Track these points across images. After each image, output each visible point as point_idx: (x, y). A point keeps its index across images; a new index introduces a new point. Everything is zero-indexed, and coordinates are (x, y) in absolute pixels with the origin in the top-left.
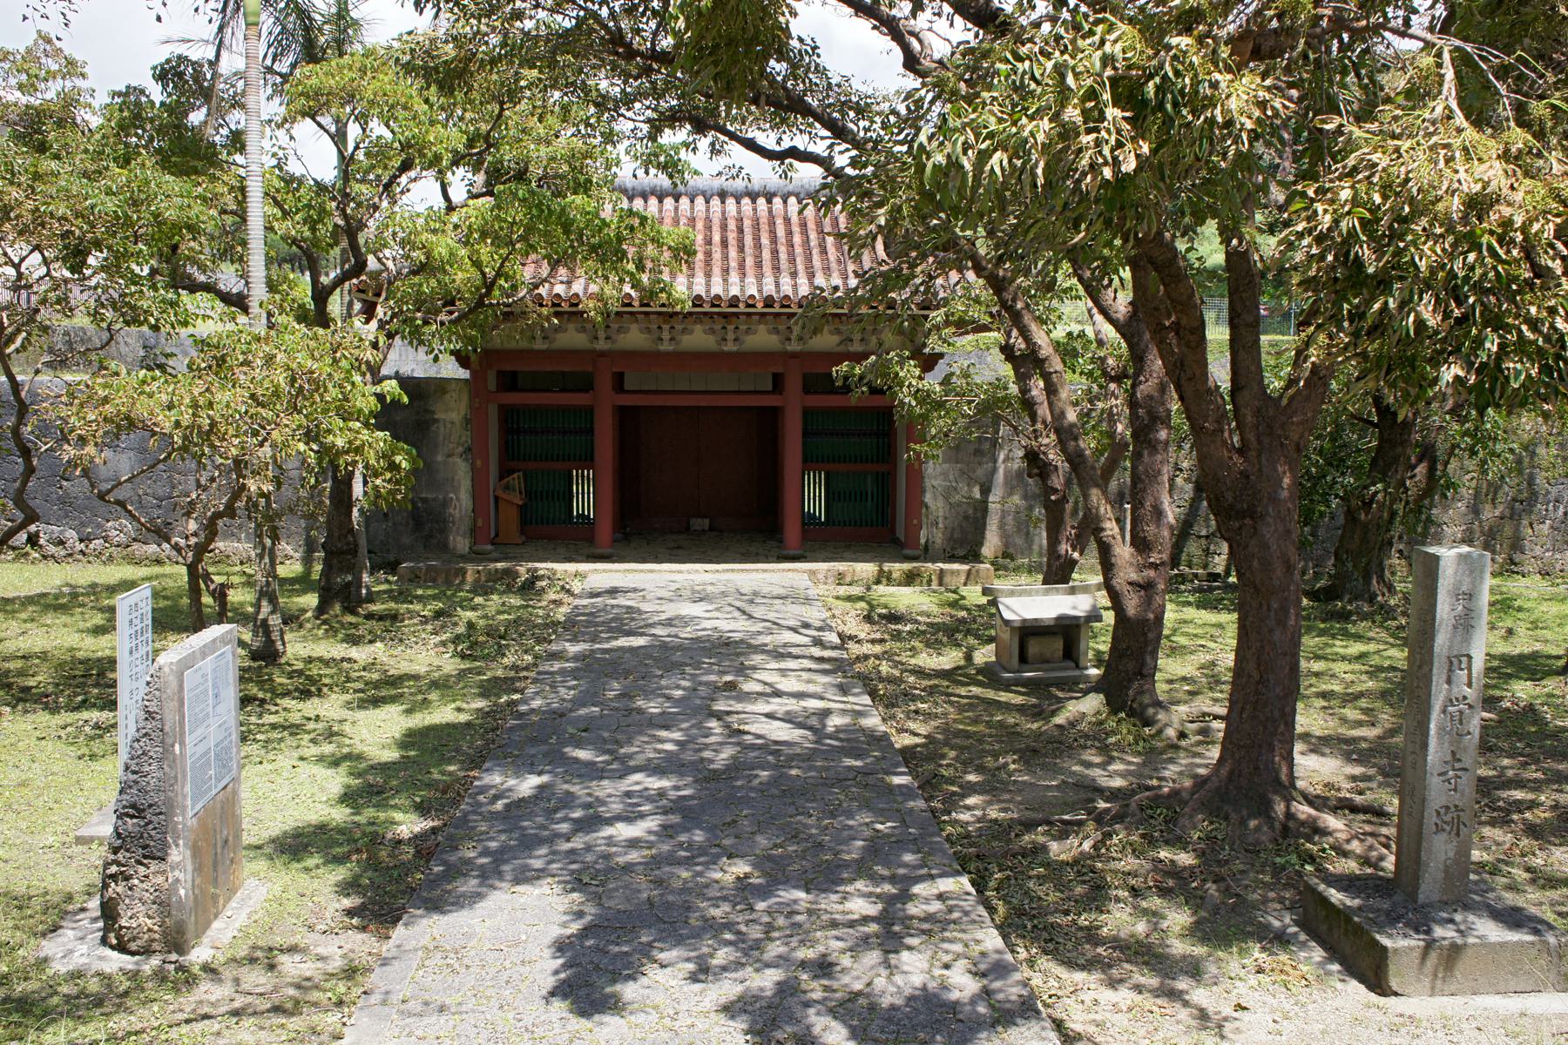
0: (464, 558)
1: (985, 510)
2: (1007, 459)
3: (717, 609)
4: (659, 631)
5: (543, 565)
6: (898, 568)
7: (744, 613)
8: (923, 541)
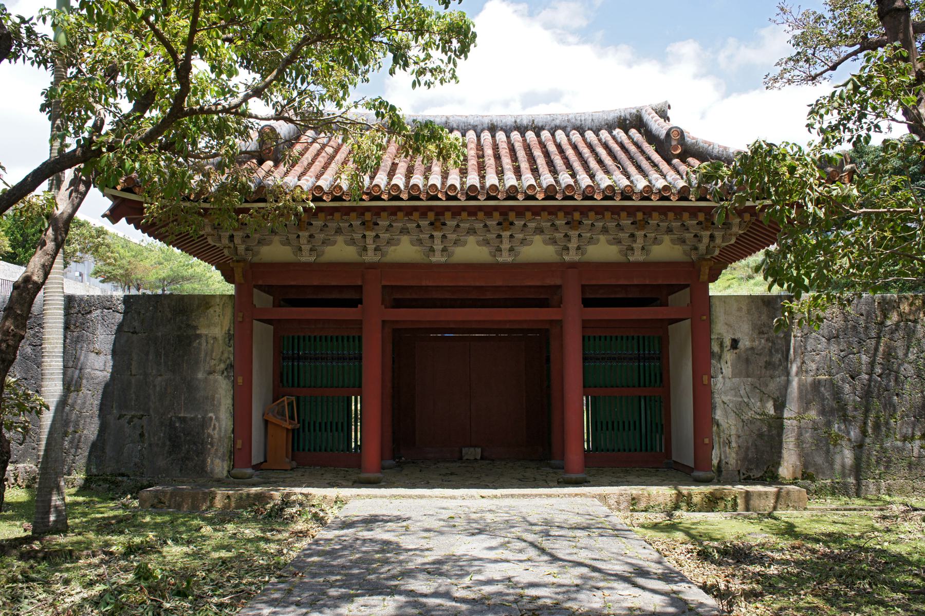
0: (220, 483)
1: (781, 427)
2: (800, 371)
3: (503, 545)
4: (420, 585)
5: (297, 490)
6: (698, 492)
7: (543, 551)
8: (715, 462)
